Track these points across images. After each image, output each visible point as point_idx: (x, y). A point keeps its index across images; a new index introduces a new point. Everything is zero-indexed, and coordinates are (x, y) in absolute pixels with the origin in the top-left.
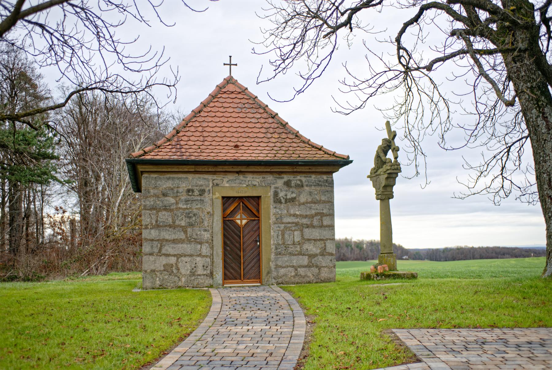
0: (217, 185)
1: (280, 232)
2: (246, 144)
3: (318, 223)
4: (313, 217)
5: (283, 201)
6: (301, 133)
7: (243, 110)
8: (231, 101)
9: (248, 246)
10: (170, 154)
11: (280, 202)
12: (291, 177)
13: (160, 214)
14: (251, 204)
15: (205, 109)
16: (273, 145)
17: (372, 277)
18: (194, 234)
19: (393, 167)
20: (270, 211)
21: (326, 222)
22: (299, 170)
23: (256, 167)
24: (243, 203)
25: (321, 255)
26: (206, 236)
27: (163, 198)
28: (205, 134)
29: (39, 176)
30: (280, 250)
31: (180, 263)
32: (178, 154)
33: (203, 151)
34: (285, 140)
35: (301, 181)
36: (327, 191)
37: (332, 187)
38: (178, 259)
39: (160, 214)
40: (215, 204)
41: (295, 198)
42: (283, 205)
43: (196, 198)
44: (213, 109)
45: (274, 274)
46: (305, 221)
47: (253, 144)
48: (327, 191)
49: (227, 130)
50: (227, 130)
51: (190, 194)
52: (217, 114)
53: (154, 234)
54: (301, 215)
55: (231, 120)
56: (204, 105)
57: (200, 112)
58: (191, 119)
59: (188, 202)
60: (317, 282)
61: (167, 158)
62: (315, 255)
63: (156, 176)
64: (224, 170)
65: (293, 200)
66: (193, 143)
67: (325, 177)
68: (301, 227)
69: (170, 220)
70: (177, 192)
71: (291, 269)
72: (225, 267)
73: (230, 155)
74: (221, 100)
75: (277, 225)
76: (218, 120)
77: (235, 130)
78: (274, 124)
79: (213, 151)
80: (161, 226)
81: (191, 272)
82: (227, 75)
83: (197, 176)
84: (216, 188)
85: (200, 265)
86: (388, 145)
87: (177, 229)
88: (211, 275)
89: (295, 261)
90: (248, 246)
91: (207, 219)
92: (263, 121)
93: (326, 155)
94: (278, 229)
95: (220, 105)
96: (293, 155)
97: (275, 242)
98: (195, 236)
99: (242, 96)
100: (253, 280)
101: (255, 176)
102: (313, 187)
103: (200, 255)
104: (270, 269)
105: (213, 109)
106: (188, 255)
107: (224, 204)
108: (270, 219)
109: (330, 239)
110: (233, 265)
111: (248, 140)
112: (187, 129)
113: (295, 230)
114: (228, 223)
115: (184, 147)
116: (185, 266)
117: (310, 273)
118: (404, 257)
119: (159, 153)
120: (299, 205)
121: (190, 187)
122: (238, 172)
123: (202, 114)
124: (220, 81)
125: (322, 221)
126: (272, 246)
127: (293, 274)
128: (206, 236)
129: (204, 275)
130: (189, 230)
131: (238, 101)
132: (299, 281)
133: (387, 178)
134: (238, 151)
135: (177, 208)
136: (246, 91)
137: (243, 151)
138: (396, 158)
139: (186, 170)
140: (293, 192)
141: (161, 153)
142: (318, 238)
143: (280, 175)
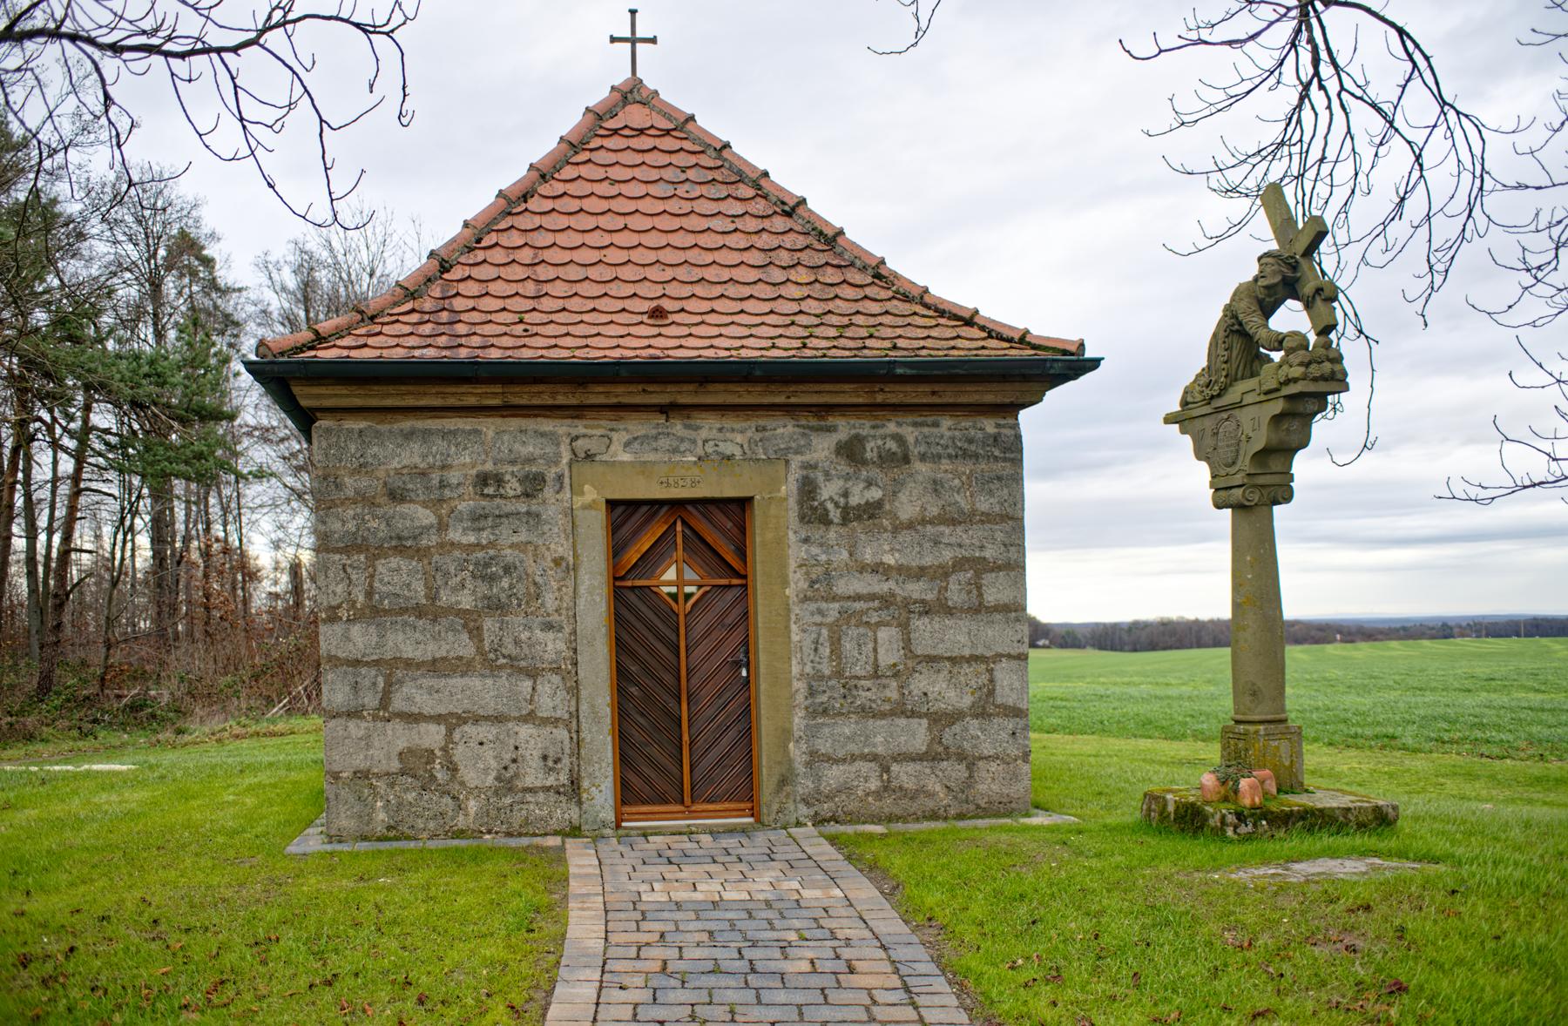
0: (589, 457)
1: (825, 632)
2: (691, 305)
3: (964, 596)
4: (946, 575)
5: (835, 515)
6: (891, 264)
7: (681, 190)
8: (638, 158)
9: (706, 682)
10: (412, 341)
11: (825, 521)
12: (864, 426)
13: (381, 567)
14: (717, 529)
15: (544, 189)
16: (795, 307)
17: (1214, 822)
18: (508, 641)
19: (1314, 370)
20: (785, 554)
21: (995, 591)
22: (893, 399)
23: (732, 387)
24: (684, 523)
25: (976, 716)
26: (553, 646)
27: (389, 509)
28: (544, 272)
29: (187, 463)
30: (824, 698)
31: (461, 748)
32: (442, 341)
33: (535, 329)
34: (838, 290)
35: (899, 439)
36: (999, 478)
37: (1018, 462)
38: (450, 732)
39: (380, 568)
40: (581, 531)
41: (879, 504)
42: (833, 529)
43: (509, 507)
44: (572, 188)
45: (805, 785)
46: (917, 590)
47: (719, 305)
48: (999, 478)
49: (622, 256)
50: (622, 256)
51: (490, 490)
52: (589, 204)
53: (360, 639)
54: (900, 569)
55: (637, 222)
56: (542, 173)
57: (525, 198)
58: (495, 220)
59: (482, 523)
60: (961, 817)
61: (398, 354)
62: (955, 717)
63: (363, 425)
64: (614, 400)
65: (871, 511)
66: (499, 304)
67: (989, 425)
68: (903, 612)
69: (419, 588)
70: (443, 485)
71: (864, 767)
72: (625, 759)
73: (637, 343)
74: (601, 157)
75: (813, 606)
76: (591, 222)
77: (652, 257)
78: (792, 236)
79: (571, 329)
80: (386, 612)
81: (498, 778)
82: (622, 75)
83: (514, 423)
84: (586, 468)
85: (532, 754)
86: (1292, 272)
87: (443, 621)
88: (574, 790)
89: (879, 739)
90: (706, 682)
91: (555, 585)
92: (751, 224)
93: (993, 343)
94: (818, 619)
95: (599, 173)
96: (869, 343)
97: (808, 669)
98: (510, 648)
99: (677, 145)
100: (727, 805)
101: (729, 422)
102: (946, 464)
103: (529, 718)
104: (791, 769)
105: (572, 188)
106: (487, 718)
107: (614, 528)
108: (785, 583)
109: (1009, 656)
110: (654, 751)
111: (699, 290)
112: (480, 255)
113: (879, 624)
114: (632, 597)
115: (464, 317)
116: (479, 757)
117: (935, 782)
118: (1041, 643)
119: (371, 341)
120: (896, 530)
121: (489, 467)
122: (666, 410)
123: (534, 204)
124: (598, 94)
125: (979, 588)
126: (797, 685)
127: (874, 784)
128: (553, 646)
129: (548, 789)
130: (489, 624)
131: (664, 159)
132: (897, 811)
133: (1277, 419)
134: (663, 331)
135: (441, 545)
136: (690, 126)
137: (685, 331)
138: (1325, 330)
139: (472, 401)
140: (870, 484)
141: (381, 338)
142: (967, 652)
143: (821, 418)
